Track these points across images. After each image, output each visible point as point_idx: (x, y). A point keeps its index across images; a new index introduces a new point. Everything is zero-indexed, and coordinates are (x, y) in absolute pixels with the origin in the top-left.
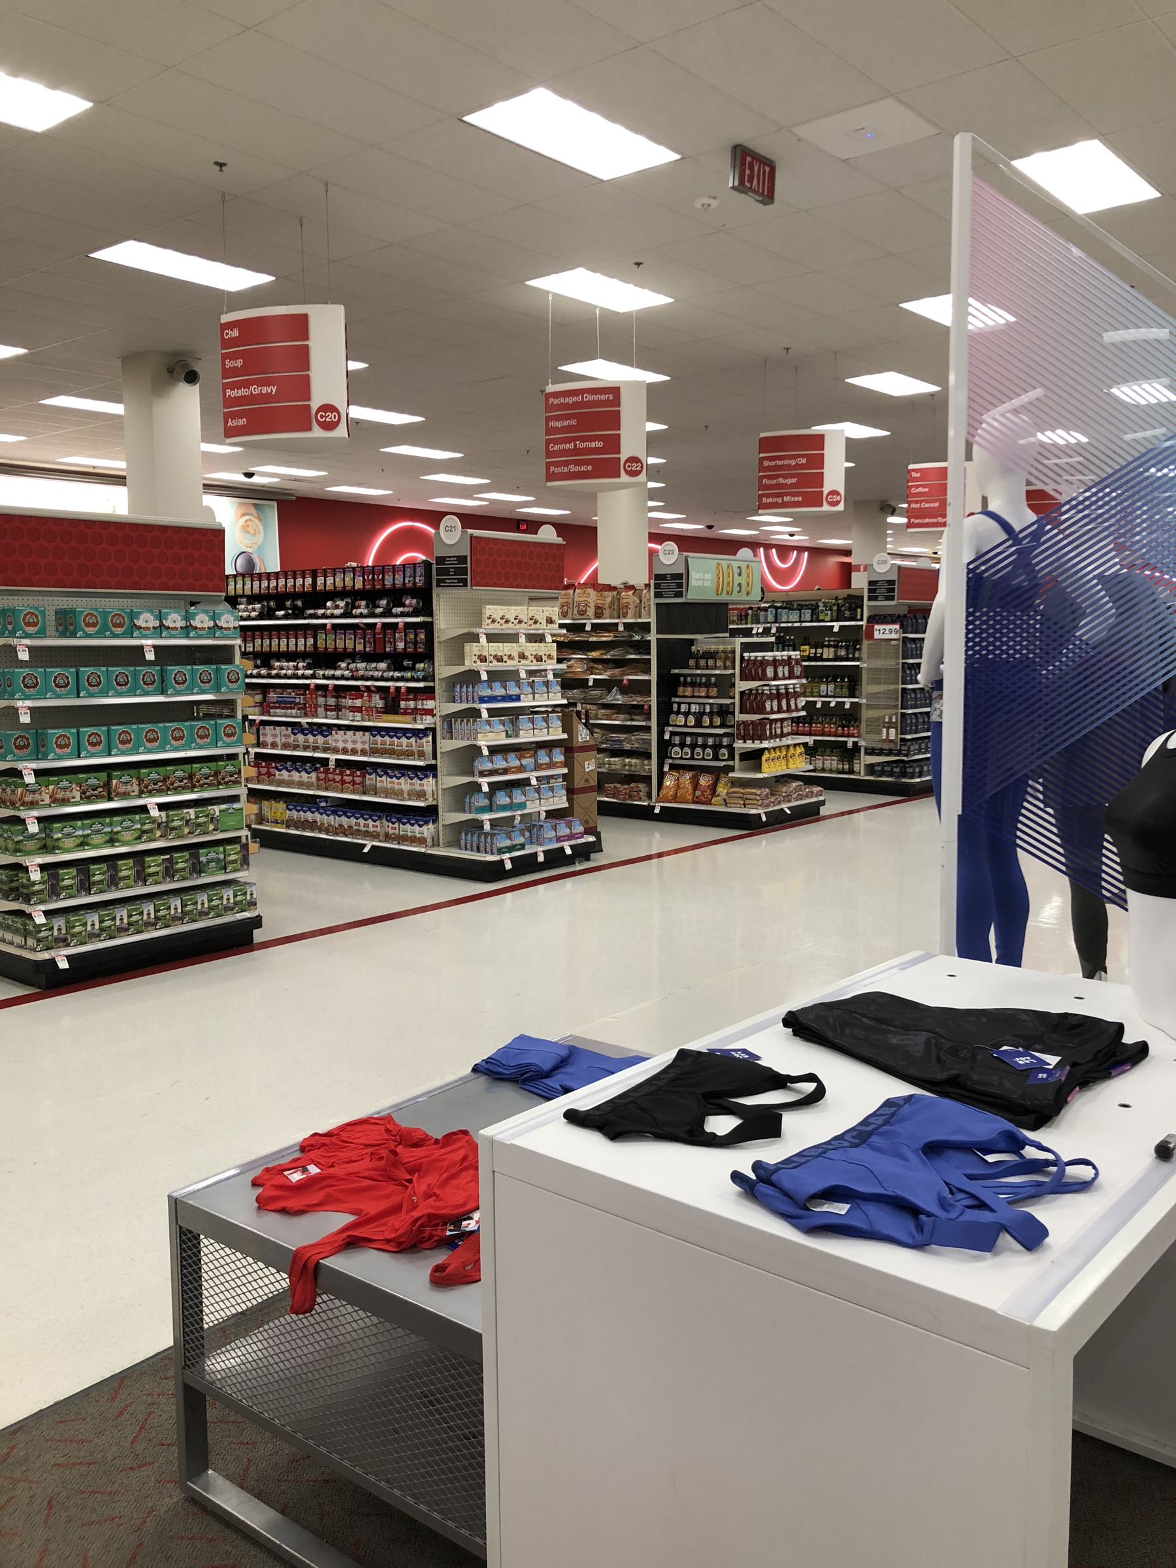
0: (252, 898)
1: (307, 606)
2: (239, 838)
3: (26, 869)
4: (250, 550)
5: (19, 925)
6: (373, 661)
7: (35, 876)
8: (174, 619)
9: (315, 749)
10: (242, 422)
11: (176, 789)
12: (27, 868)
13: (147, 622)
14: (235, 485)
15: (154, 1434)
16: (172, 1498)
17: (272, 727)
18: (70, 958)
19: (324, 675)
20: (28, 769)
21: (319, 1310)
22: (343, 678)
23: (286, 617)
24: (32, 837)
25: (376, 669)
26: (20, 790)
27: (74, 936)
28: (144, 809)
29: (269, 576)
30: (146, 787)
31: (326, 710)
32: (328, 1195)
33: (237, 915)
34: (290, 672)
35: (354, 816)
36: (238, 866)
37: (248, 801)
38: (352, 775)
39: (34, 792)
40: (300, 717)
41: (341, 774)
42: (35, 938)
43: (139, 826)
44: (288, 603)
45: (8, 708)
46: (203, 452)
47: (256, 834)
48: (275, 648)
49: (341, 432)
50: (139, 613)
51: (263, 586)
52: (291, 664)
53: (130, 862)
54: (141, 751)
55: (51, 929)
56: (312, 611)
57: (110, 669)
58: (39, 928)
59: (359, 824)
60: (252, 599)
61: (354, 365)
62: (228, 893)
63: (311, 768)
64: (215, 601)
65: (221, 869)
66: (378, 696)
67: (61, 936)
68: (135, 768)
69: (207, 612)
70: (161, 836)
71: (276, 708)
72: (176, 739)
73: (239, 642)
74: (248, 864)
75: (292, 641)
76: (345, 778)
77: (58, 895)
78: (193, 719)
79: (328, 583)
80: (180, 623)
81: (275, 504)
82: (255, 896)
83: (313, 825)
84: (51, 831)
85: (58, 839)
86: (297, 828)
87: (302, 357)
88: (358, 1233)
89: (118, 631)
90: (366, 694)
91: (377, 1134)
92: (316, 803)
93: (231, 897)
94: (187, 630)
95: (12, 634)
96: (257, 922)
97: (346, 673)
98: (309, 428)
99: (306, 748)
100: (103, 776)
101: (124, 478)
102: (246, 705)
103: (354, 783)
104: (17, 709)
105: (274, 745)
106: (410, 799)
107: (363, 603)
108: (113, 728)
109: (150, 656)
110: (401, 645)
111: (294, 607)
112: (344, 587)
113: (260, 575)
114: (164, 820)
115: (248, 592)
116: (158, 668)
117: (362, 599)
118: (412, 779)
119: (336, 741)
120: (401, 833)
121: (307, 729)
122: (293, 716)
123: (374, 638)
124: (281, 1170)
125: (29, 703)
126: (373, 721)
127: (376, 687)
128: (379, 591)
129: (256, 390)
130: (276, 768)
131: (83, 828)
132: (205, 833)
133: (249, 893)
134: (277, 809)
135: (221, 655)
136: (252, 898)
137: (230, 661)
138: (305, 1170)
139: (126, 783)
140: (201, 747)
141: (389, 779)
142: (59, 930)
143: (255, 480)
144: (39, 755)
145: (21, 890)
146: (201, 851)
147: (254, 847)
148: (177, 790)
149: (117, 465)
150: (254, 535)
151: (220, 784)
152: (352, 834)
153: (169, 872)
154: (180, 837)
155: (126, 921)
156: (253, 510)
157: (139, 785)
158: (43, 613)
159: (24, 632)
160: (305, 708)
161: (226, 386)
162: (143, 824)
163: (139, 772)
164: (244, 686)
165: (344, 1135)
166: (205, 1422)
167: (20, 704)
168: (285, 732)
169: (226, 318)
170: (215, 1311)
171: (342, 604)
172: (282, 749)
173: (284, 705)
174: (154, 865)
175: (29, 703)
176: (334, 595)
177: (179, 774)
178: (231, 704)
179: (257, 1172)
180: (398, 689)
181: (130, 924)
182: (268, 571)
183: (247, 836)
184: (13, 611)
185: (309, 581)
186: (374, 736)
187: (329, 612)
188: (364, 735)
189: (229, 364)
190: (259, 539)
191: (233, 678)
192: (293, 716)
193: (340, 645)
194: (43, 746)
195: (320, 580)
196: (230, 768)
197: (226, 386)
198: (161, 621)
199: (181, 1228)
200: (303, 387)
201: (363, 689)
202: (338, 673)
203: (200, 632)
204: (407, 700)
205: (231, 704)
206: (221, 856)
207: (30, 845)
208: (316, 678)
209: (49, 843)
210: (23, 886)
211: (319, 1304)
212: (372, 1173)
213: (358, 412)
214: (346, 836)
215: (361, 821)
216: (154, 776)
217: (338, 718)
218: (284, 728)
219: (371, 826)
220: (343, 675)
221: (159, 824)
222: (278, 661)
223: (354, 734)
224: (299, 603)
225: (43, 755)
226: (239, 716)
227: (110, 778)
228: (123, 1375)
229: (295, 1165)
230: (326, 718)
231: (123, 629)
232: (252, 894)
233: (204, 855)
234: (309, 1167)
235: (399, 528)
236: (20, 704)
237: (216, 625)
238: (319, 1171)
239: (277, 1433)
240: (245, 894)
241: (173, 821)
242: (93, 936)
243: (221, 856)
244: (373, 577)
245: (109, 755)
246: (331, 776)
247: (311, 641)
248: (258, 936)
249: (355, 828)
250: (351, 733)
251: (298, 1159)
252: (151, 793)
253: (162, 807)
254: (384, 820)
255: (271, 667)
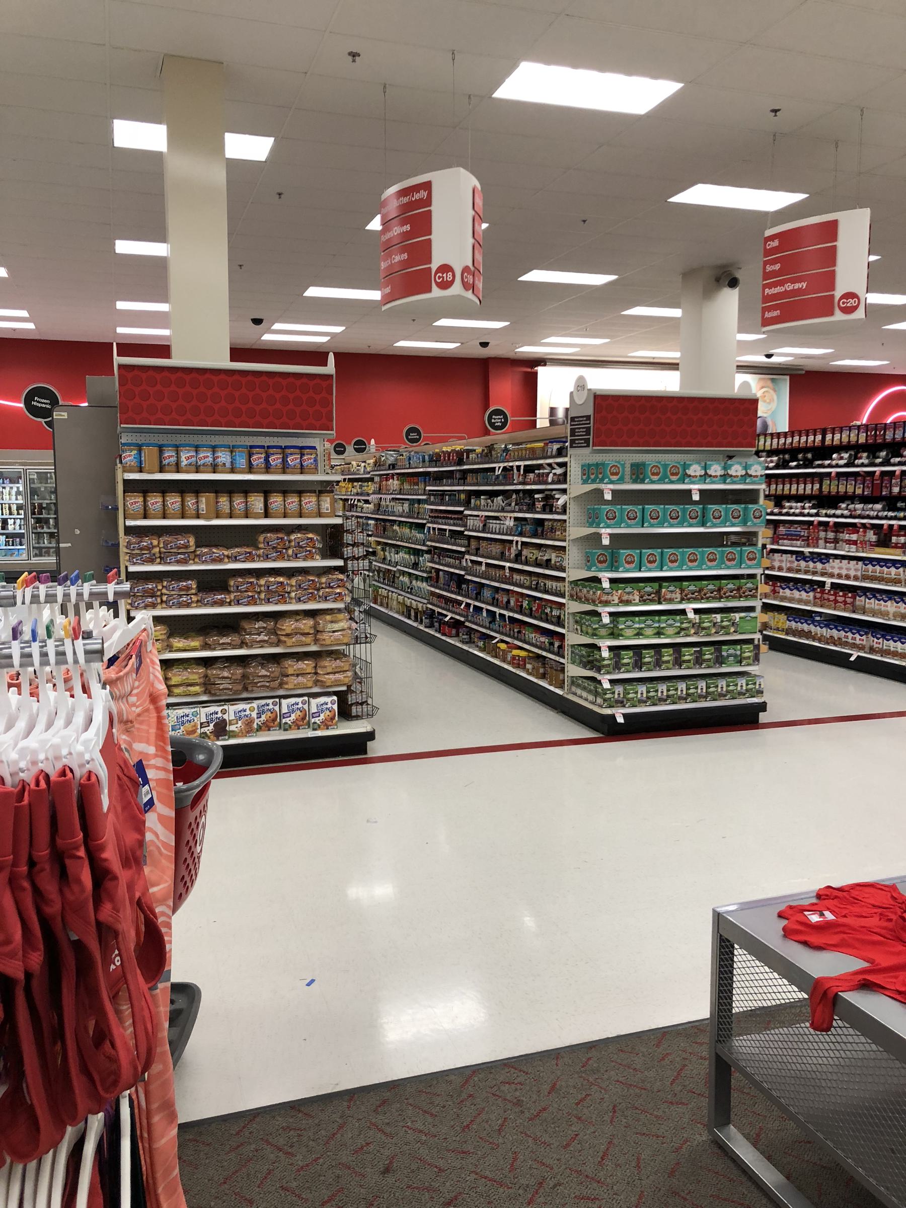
0: (760, 687)
1: (815, 458)
2: (753, 640)
3: (599, 649)
4: (765, 415)
5: (592, 688)
6: (870, 503)
7: (605, 654)
8: (716, 469)
9: (814, 573)
10: (776, 313)
11: (707, 598)
12: (600, 648)
13: (716, 471)
14: (760, 365)
15: (688, 1083)
16: (701, 1137)
17: (780, 554)
18: (625, 716)
19: (826, 514)
20: (605, 576)
21: (834, 1033)
22: (842, 516)
23: (797, 467)
24: (604, 626)
25: (872, 509)
26: (599, 592)
27: (628, 700)
28: (683, 612)
29: (778, 435)
30: (686, 596)
31: (826, 542)
32: (843, 939)
33: (748, 699)
34: (798, 511)
35: (843, 630)
36: (751, 661)
37: (762, 612)
38: (844, 596)
39: (608, 594)
40: (803, 547)
41: (835, 595)
42: (602, 698)
43: (679, 624)
44: (800, 456)
45: (594, 533)
46: (739, 342)
47: (766, 638)
48: (786, 492)
49: (860, 314)
50: (690, 465)
51: (780, 442)
52: (799, 504)
53: (671, 651)
54: (684, 568)
55: (613, 693)
56: (819, 462)
57: (666, 507)
58: (605, 691)
59: (847, 637)
60: (771, 453)
61: (873, 258)
62: (742, 682)
63: (809, 588)
64: (747, 455)
65: (737, 663)
66: (872, 532)
67: (620, 699)
68: (717, 580)
69: (740, 463)
70: (694, 633)
71: (784, 539)
72: (691, 561)
73: (763, 486)
74: (758, 661)
75: (802, 486)
76: (838, 598)
77: (619, 669)
78: (723, 546)
79: (835, 439)
80: (720, 472)
81: (788, 378)
82: (762, 686)
83: (808, 635)
84: (618, 623)
85: (622, 629)
86: (794, 636)
87: (831, 256)
88: (871, 978)
89: (674, 478)
90: (861, 530)
91: (886, 900)
92: (812, 617)
93: (744, 685)
94: (725, 477)
95: (601, 481)
96: (763, 707)
97: (846, 512)
98: (832, 313)
99: (806, 572)
100: (656, 585)
101: (678, 364)
102: (764, 535)
103: (845, 603)
104: (601, 535)
105: (780, 569)
106: (895, 620)
107: (865, 455)
108: (666, 550)
109: (696, 497)
110: (896, 490)
111: (805, 459)
112: (849, 442)
113: (772, 435)
114: (697, 621)
115: (768, 448)
116: (701, 506)
117: (864, 452)
118: (897, 603)
119: (833, 568)
120: (885, 647)
121: (809, 557)
122: (797, 546)
123: (873, 482)
124: (801, 910)
125: (609, 531)
126: (866, 552)
127: (871, 524)
128: (880, 444)
129: (789, 287)
130: (781, 586)
131: (639, 623)
132: (728, 634)
133: (758, 683)
134: (781, 620)
135: (749, 497)
136: (760, 687)
137: (755, 501)
138: (822, 915)
139: (672, 592)
140: (729, 568)
141: (877, 602)
142: (619, 694)
143: (774, 360)
144: (613, 568)
145: (595, 663)
146: (723, 647)
147: (764, 648)
148: (708, 600)
149: (673, 355)
150: (769, 403)
151: (741, 597)
152: (841, 644)
153: (699, 661)
154: (709, 635)
155: (665, 694)
156: (769, 383)
157: (681, 594)
158: (623, 466)
159: (610, 479)
160: (808, 540)
161: (765, 287)
162: (682, 623)
163: (682, 585)
164: (765, 521)
165: (854, 893)
166: (730, 1088)
167: (603, 531)
168: (790, 559)
169: (768, 233)
170: (741, 1003)
171: (846, 456)
172: (786, 572)
173: (791, 537)
174: (688, 655)
175: (609, 531)
176: (840, 448)
177: (711, 587)
178: (755, 534)
179: (782, 907)
180: (891, 526)
181: (668, 696)
182: (779, 431)
183: (759, 639)
184: (603, 464)
185: (819, 438)
186: (866, 565)
187: (834, 463)
188: (857, 564)
189: (769, 268)
190: (773, 406)
191: (757, 514)
192: (797, 546)
193: (842, 489)
194: (616, 562)
195: (829, 437)
196: (750, 585)
197: (765, 287)
198: (706, 471)
199: (721, 936)
200: (830, 280)
201: (859, 525)
202: (839, 512)
203: (735, 479)
204: (898, 536)
205: (755, 534)
206: (738, 653)
207: (603, 632)
208: (819, 516)
209: (615, 631)
210: (597, 660)
211: (835, 1027)
212: (883, 932)
213: (875, 298)
214: (835, 645)
215: (850, 635)
216: (692, 588)
217: (835, 549)
218: (789, 555)
219: (858, 639)
220: (842, 514)
221: (694, 624)
222: (789, 502)
223: (849, 563)
224: (809, 456)
225: (616, 568)
226: (760, 545)
227: (661, 587)
228: (665, 1030)
229: (812, 908)
230: (825, 548)
231: (678, 477)
232: (760, 685)
233: (726, 651)
234: (825, 912)
235: (899, 390)
236: (603, 531)
237: (747, 473)
238: (834, 918)
239: (792, 1117)
240: (755, 684)
241: (704, 622)
242: (641, 702)
243: (738, 653)
244: (876, 433)
245: (661, 570)
246: (826, 596)
247: (817, 486)
248: (763, 717)
249: (844, 640)
250: (846, 561)
251: (816, 904)
252: (689, 600)
253: (697, 611)
254: (870, 635)
255: (782, 507)
